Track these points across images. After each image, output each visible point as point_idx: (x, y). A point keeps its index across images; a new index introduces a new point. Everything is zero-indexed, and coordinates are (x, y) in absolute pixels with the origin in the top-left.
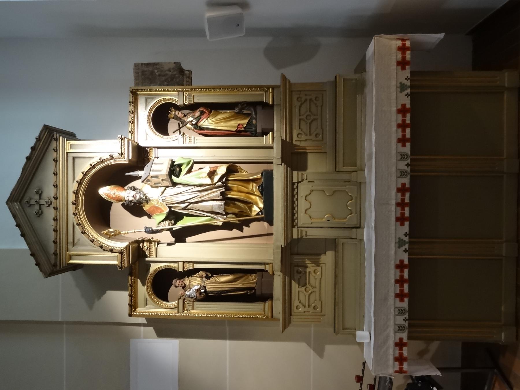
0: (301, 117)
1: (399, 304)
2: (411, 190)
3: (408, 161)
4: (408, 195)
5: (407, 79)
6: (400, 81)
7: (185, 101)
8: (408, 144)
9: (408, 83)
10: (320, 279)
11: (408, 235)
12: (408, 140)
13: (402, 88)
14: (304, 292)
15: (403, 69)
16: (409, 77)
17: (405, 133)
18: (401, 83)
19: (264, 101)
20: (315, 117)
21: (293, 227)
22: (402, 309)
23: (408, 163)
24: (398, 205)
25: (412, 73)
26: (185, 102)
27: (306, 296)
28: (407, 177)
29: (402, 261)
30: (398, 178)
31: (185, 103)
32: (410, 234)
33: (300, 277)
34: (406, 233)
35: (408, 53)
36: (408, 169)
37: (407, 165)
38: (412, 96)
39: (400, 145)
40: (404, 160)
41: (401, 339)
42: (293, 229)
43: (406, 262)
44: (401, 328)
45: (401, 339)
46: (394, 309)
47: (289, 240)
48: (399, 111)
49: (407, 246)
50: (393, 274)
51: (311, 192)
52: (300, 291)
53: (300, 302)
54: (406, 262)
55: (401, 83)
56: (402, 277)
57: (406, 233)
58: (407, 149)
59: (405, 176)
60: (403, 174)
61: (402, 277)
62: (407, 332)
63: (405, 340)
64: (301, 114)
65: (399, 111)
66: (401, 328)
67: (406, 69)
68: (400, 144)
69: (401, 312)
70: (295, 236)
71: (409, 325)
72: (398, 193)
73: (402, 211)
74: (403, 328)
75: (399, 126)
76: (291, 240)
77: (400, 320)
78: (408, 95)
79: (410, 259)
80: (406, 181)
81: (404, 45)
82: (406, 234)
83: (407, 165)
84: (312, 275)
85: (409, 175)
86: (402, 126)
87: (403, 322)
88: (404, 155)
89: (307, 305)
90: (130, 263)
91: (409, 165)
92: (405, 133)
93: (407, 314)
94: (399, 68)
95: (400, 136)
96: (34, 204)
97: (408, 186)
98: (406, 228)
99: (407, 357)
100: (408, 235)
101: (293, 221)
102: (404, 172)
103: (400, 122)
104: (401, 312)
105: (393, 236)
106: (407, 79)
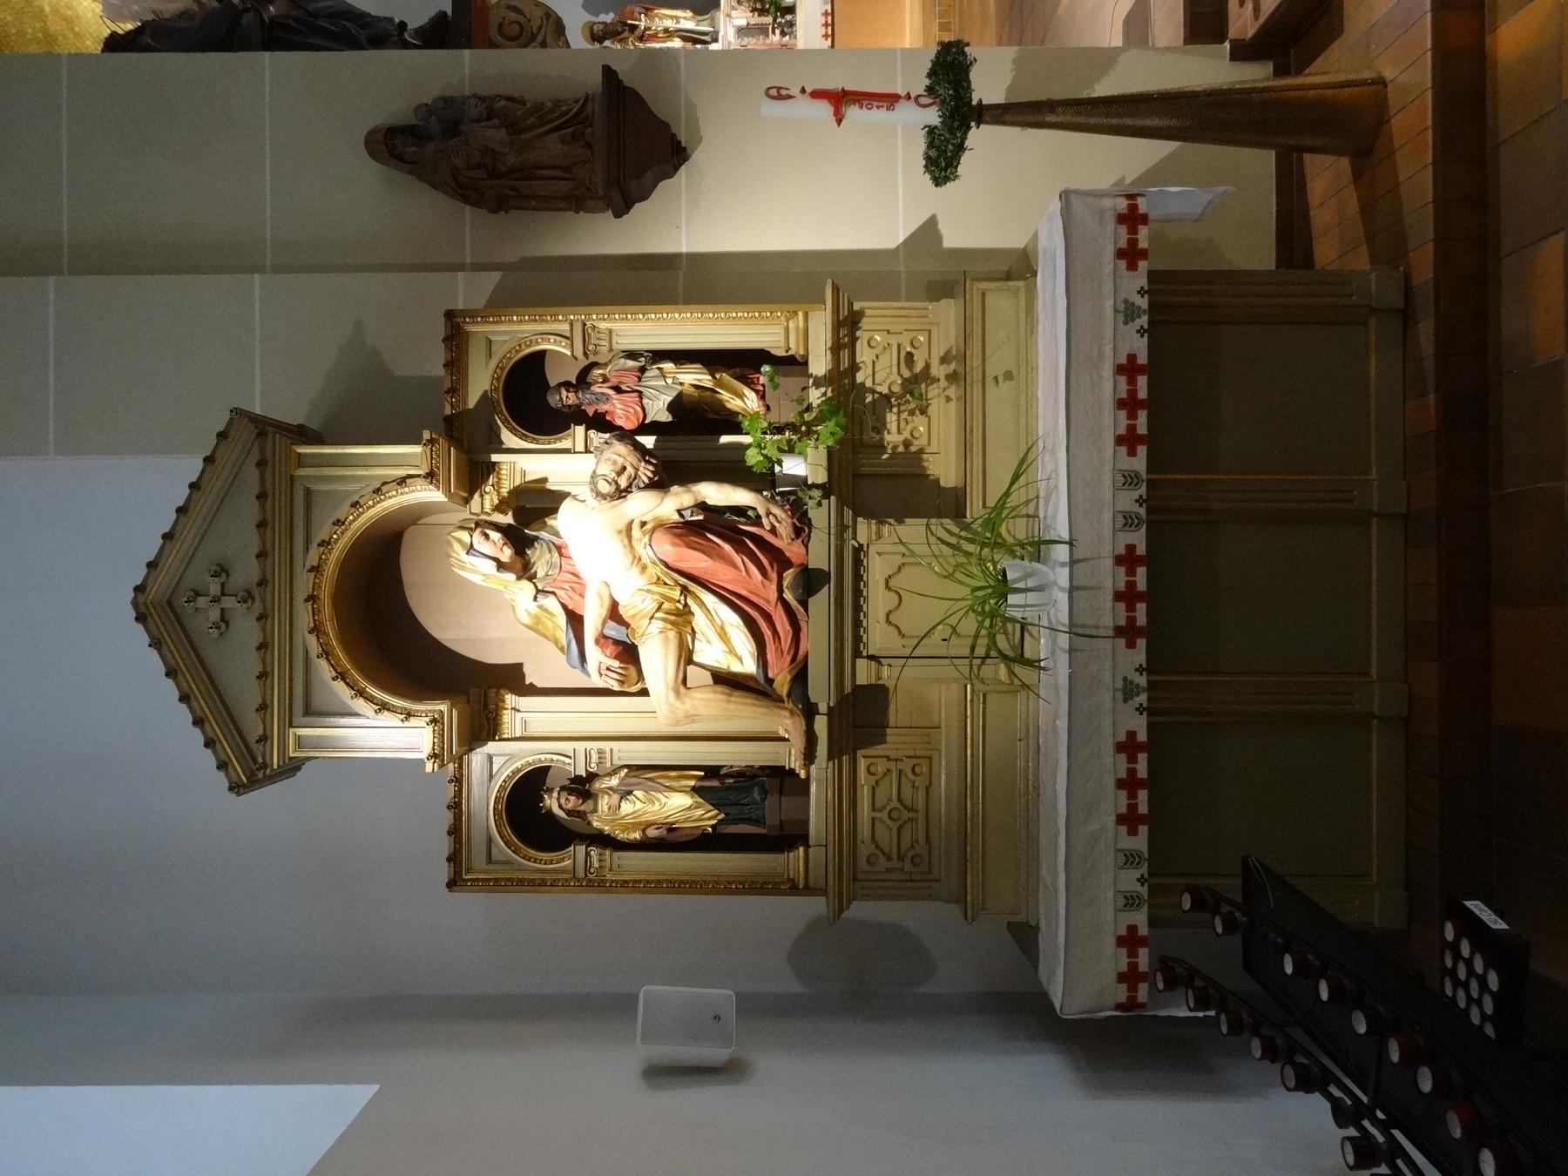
0: (877, 815)
1: (1128, 843)
2: (1149, 560)
3: (1140, 490)
4: (1143, 796)
5: (1141, 292)
6: (1124, 296)
7: (590, 867)
8: (1143, 830)
9: (1143, 303)
10: (928, 788)
11: (1145, 331)
12: (1142, 820)
13: (1130, 313)
14: (889, 822)
15: (1132, 266)
16: (1145, 706)
17: (1135, 801)
18: (1125, 679)
19: (785, 767)
20: (911, 815)
21: (857, 654)
22: (1134, 894)
23: (1141, 497)
24: (1118, 596)
25: (1153, 276)
26: (591, 874)
27: (891, 829)
28: (1138, 530)
29: (1132, 735)
30: (1118, 910)
31: (588, 768)
32: (1151, 668)
33: (877, 782)
34: (1141, 705)
35: (1141, 571)
36: (1144, 891)
37: (1141, 880)
38: (1153, 332)
39: (1123, 829)
40: (1130, 487)
41: (1132, 929)
42: (857, 660)
43: (1142, 737)
44: (1131, 902)
45: (1132, 929)
46: (1114, 515)
47: (848, 688)
48: (1120, 748)
49: (1144, 321)
50: (1112, 765)
51: (900, 568)
52: (877, 818)
53: (877, 846)
54: (1142, 737)
55: (1126, 301)
56: (1131, 585)
57: (1141, 665)
58: (1139, 463)
59: (1136, 526)
60: (1129, 521)
61: (1132, 772)
62: (1145, 908)
63: (1143, 930)
64: (878, 805)
65: (1120, 748)
66: (1131, 902)
67: (1138, 610)
68: (1123, 450)
69: (1130, 858)
70: (862, 680)
71: (1153, 891)
72: (1119, 827)
73: (1131, 234)
74: (1136, 521)
75: (1120, 784)
76: (853, 689)
77: (1130, 880)
78: (1142, 331)
79: (1151, 727)
80: (1139, 539)
81: (1133, 208)
82: (1142, 331)
83: (1141, 880)
84: (908, 779)
85: (1146, 904)
86: (1129, 784)
87: (1136, 508)
88: (1132, 478)
89: (895, 856)
90: (454, 753)
91: (1146, 292)
92: (1135, 801)
93: (1146, 864)
94: (1123, 264)
95: (1122, 430)
96: (222, 609)
97: (1141, 549)
98: (1139, 655)
99: (1147, 250)
100: (1145, 331)
101: (857, 639)
102: (1131, 518)
103: (1123, 774)
104: (1130, 858)
105: (1109, 731)
106: (1141, 292)
